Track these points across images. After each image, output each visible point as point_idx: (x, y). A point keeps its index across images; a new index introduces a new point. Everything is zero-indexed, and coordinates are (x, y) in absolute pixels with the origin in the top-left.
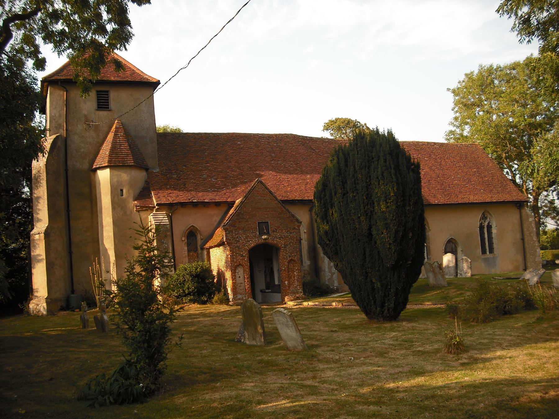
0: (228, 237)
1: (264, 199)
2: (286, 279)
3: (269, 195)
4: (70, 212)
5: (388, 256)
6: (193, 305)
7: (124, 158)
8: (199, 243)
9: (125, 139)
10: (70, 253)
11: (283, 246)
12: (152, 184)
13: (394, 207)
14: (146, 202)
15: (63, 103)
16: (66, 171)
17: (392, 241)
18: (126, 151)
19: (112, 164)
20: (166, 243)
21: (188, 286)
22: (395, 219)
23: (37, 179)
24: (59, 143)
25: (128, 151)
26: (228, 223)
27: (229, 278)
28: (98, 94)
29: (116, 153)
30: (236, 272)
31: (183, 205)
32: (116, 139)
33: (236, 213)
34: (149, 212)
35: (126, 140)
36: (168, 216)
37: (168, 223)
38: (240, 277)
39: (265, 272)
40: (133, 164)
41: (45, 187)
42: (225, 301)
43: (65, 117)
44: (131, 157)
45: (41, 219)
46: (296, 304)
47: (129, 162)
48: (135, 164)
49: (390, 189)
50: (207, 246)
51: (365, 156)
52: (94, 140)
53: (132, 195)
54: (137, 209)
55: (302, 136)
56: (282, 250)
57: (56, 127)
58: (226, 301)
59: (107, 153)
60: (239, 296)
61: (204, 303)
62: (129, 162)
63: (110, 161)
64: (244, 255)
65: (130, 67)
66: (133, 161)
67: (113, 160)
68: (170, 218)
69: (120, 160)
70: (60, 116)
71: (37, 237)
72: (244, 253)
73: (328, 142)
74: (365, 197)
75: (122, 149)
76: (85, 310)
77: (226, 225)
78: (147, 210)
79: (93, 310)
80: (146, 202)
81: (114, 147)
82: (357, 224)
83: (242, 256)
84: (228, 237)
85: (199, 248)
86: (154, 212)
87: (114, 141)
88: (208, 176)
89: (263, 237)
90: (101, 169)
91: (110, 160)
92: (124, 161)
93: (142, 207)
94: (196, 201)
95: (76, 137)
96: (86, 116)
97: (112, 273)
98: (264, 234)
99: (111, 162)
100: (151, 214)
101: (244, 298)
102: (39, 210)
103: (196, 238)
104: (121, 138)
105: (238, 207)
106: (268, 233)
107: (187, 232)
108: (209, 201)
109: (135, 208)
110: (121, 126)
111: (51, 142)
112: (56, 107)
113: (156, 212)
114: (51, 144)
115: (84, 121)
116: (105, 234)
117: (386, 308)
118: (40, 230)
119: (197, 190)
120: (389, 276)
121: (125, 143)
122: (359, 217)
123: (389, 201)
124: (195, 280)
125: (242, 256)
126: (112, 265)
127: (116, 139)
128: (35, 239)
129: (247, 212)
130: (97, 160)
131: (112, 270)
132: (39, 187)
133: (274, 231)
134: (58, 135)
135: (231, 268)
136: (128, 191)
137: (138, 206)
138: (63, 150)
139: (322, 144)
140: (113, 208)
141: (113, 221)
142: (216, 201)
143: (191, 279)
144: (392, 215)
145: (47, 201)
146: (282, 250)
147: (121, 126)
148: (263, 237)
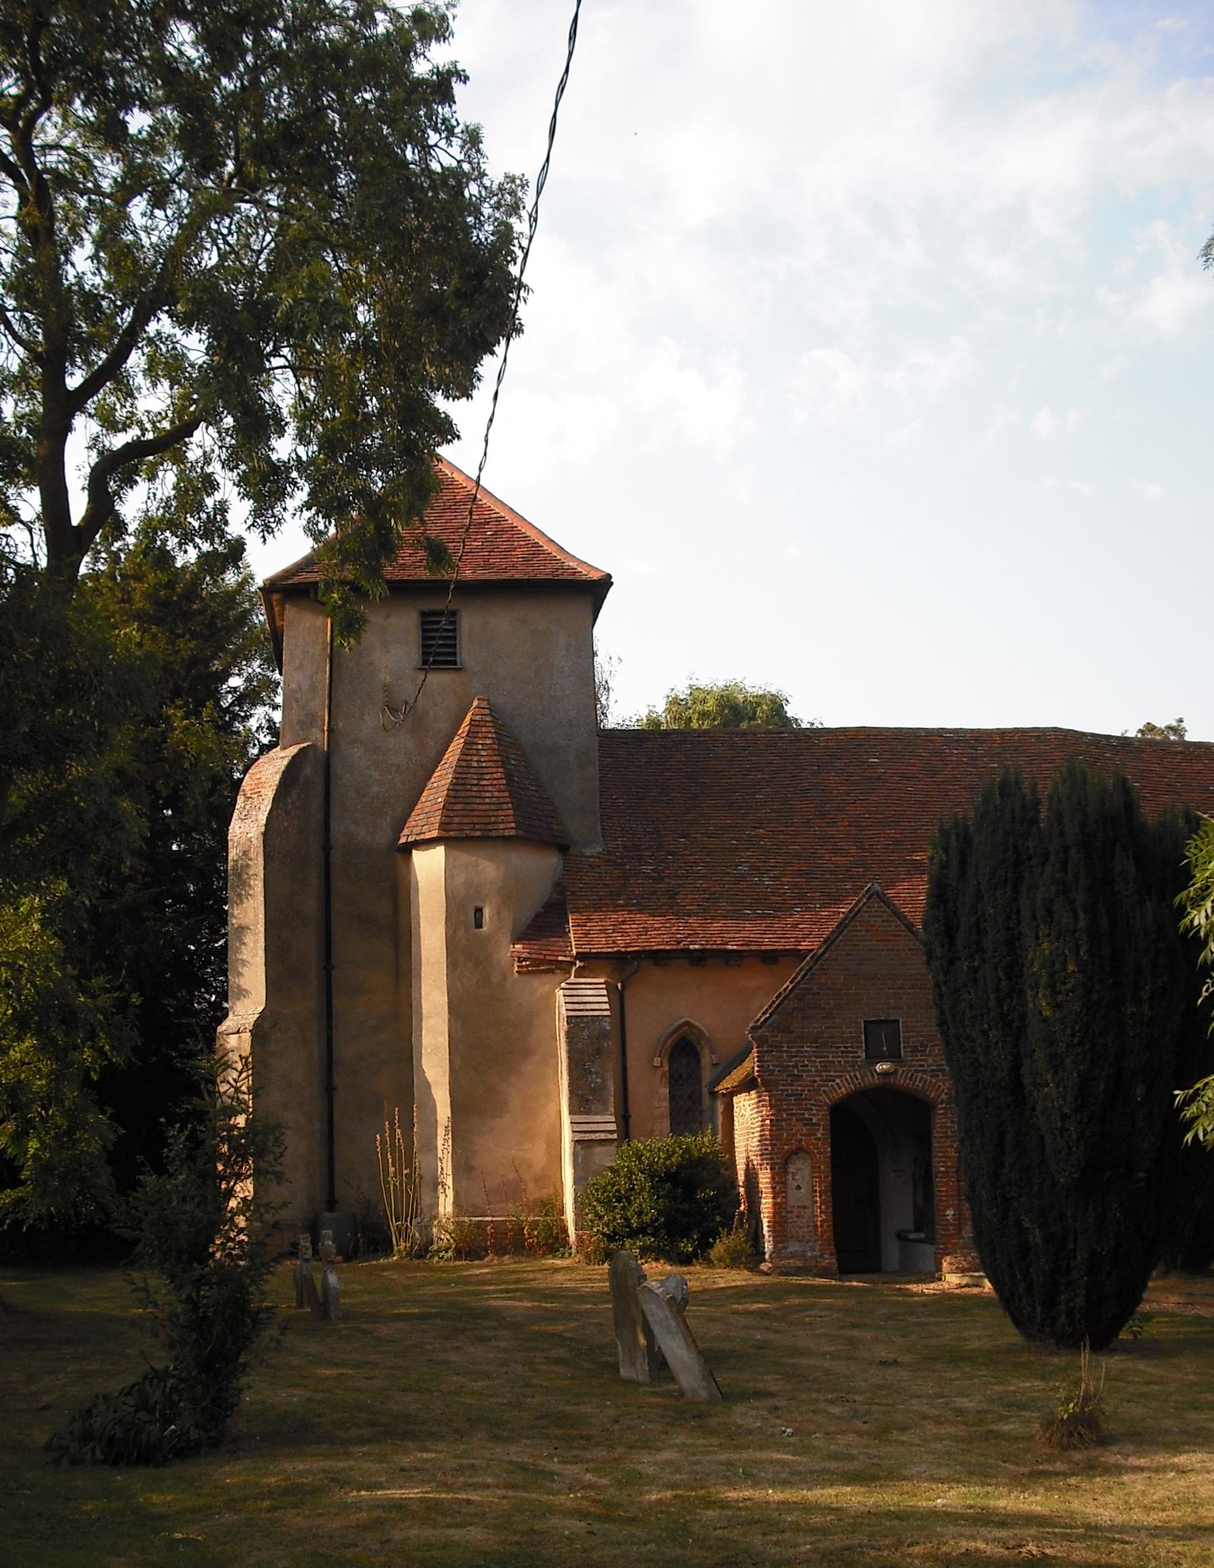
0: (766, 1064)
1: (888, 950)
2: (947, 1201)
3: (906, 936)
4: (333, 973)
5: (1060, 1153)
6: (654, 1264)
7: (487, 813)
8: (707, 1075)
9: (494, 758)
10: (329, 1090)
11: (943, 1096)
12: (574, 893)
13: (1077, 1006)
14: (549, 948)
15: (324, 649)
16: (327, 849)
17: (1071, 1109)
18: (496, 794)
19: (452, 833)
20: (597, 1073)
21: (640, 1205)
22: (1080, 1043)
23: (239, 876)
24: (308, 770)
25: (501, 794)
26: (767, 1019)
27: (766, 1188)
28: (424, 623)
29: (465, 800)
30: (787, 1173)
31: (658, 958)
32: (469, 758)
33: (796, 991)
34: (559, 976)
35: (499, 758)
36: (610, 988)
37: (608, 1013)
38: (799, 1188)
39: (914, 1175)
40: (513, 832)
41: (261, 898)
42: (746, 1258)
43: (327, 688)
44: (510, 812)
45: (246, 990)
46: (965, 1281)
47: (501, 826)
48: (521, 833)
49: (1066, 951)
50: (727, 1084)
51: (1005, 851)
52: (411, 760)
53: (509, 925)
54: (522, 967)
55: (1093, 735)
56: (941, 1109)
57: (300, 722)
58: (751, 1256)
59: (440, 800)
60: (793, 1247)
61: (685, 1260)
62: (501, 826)
63: (448, 824)
64: (814, 1121)
65: (528, 534)
66: (513, 825)
67: (457, 820)
68: (616, 996)
69: (476, 820)
70: (313, 688)
71: (232, 1041)
72: (814, 1115)
73: (1181, 752)
74: (1001, 974)
75: (486, 788)
76: (306, 1257)
77: (760, 1027)
78: (551, 971)
79: (381, 1261)
80: (549, 948)
81: (460, 781)
82: (979, 1050)
83: (808, 1123)
84: (766, 1064)
85: (705, 1090)
86: (572, 979)
87: (464, 764)
88: (753, 868)
89: (879, 1067)
90: (424, 847)
91: (447, 820)
92: (486, 824)
93: (536, 962)
94: (697, 947)
95: (358, 751)
96: (387, 689)
97: (440, 1155)
98: (882, 1058)
99: (449, 827)
100: (563, 985)
101: (809, 1254)
102: (244, 963)
103: (699, 1061)
104: (483, 753)
105: (803, 973)
106: (893, 1055)
107: (670, 1041)
108: (740, 948)
109: (516, 964)
110: (488, 718)
111: (283, 768)
112: (301, 666)
113: (575, 977)
114: (284, 772)
115: (380, 704)
116: (426, 1040)
117: (1063, 1307)
118: (243, 1022)
119: (707, 912)
120: (1069, 1214)
121: (494, 770)
122: (985, 1033)
123: (1063, 988)
124: (663, 1189)
125: (808, 1123)
126: (441, 1131)
127: (469, 758)
128: (229, 1046)
129: (829, 989)
130: (411, 822)
131: (440, 1147)
132: (244, 898)
133: (915, 1050)
134: (305, 745)
135: (772, 1159)
136: (498, 914)
137: (525, 959)
138: (320, 789)
139: (1161, 759)
140: (452, 965)
141: (449, 1003)
142: (763, 948)
143: (652, 1187)
144: (1068, 1032)
145: (263, 940)
146: (941, 1109)
147: (488, 718)
148: (879, 1067)
